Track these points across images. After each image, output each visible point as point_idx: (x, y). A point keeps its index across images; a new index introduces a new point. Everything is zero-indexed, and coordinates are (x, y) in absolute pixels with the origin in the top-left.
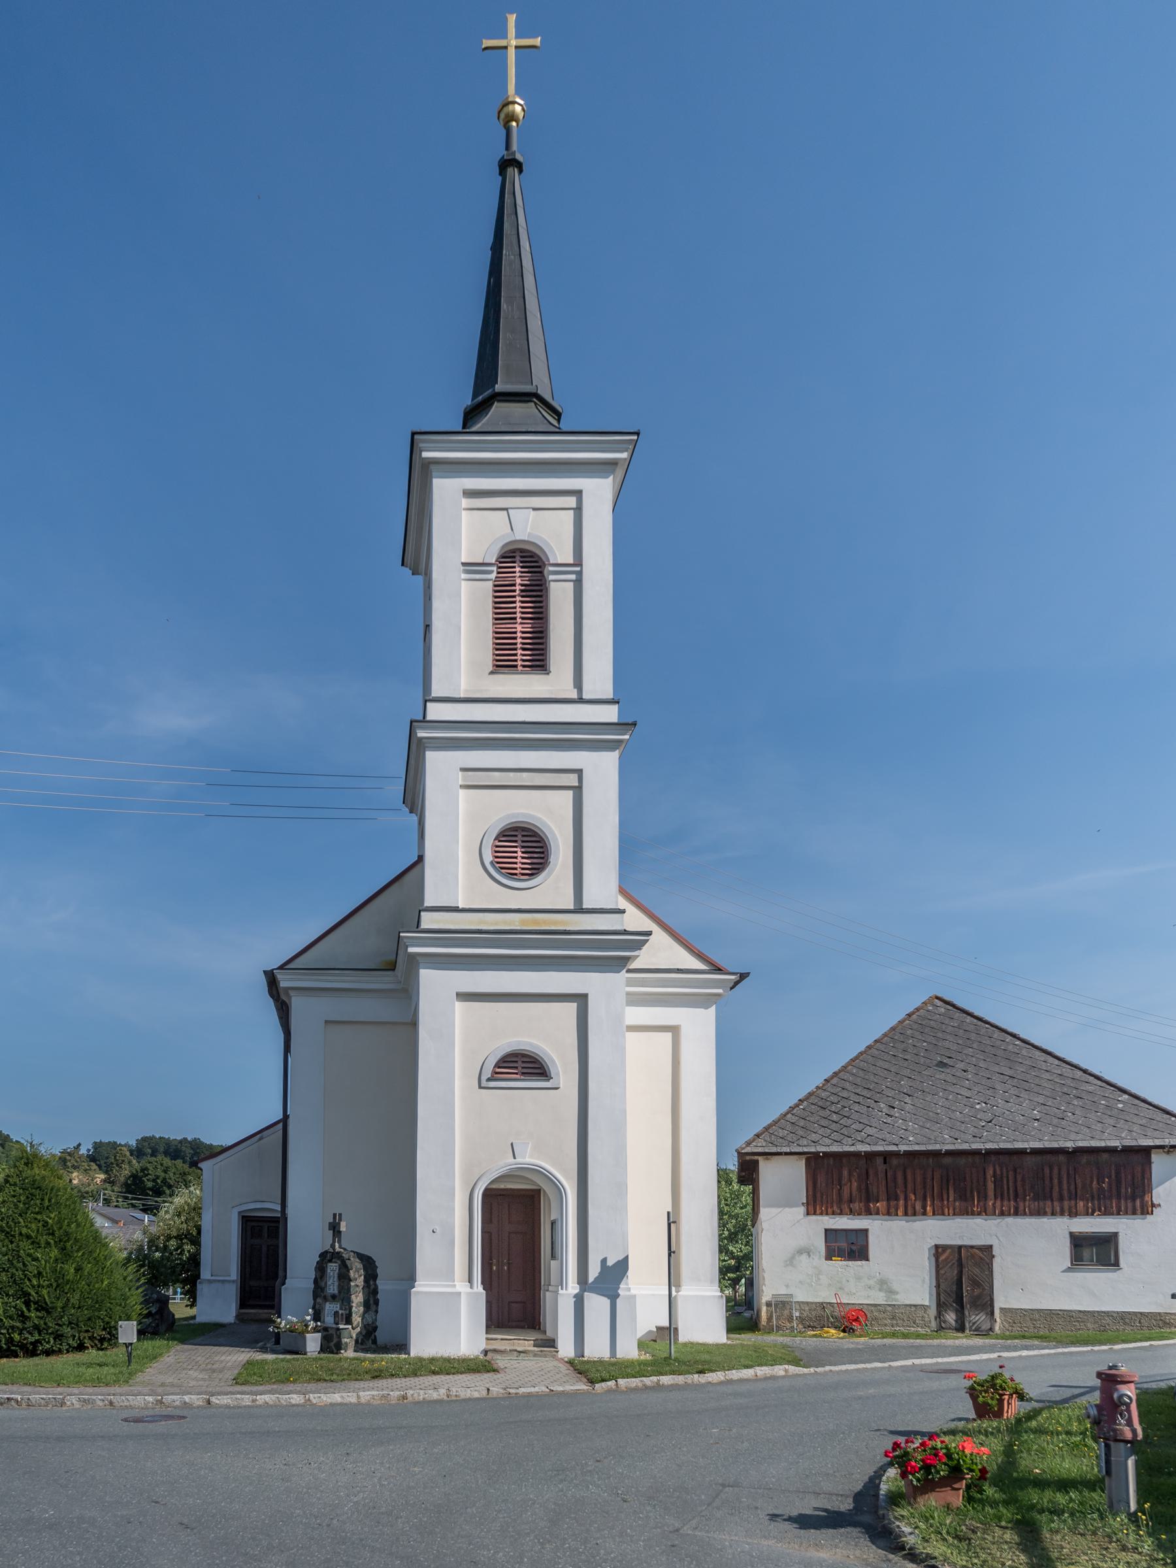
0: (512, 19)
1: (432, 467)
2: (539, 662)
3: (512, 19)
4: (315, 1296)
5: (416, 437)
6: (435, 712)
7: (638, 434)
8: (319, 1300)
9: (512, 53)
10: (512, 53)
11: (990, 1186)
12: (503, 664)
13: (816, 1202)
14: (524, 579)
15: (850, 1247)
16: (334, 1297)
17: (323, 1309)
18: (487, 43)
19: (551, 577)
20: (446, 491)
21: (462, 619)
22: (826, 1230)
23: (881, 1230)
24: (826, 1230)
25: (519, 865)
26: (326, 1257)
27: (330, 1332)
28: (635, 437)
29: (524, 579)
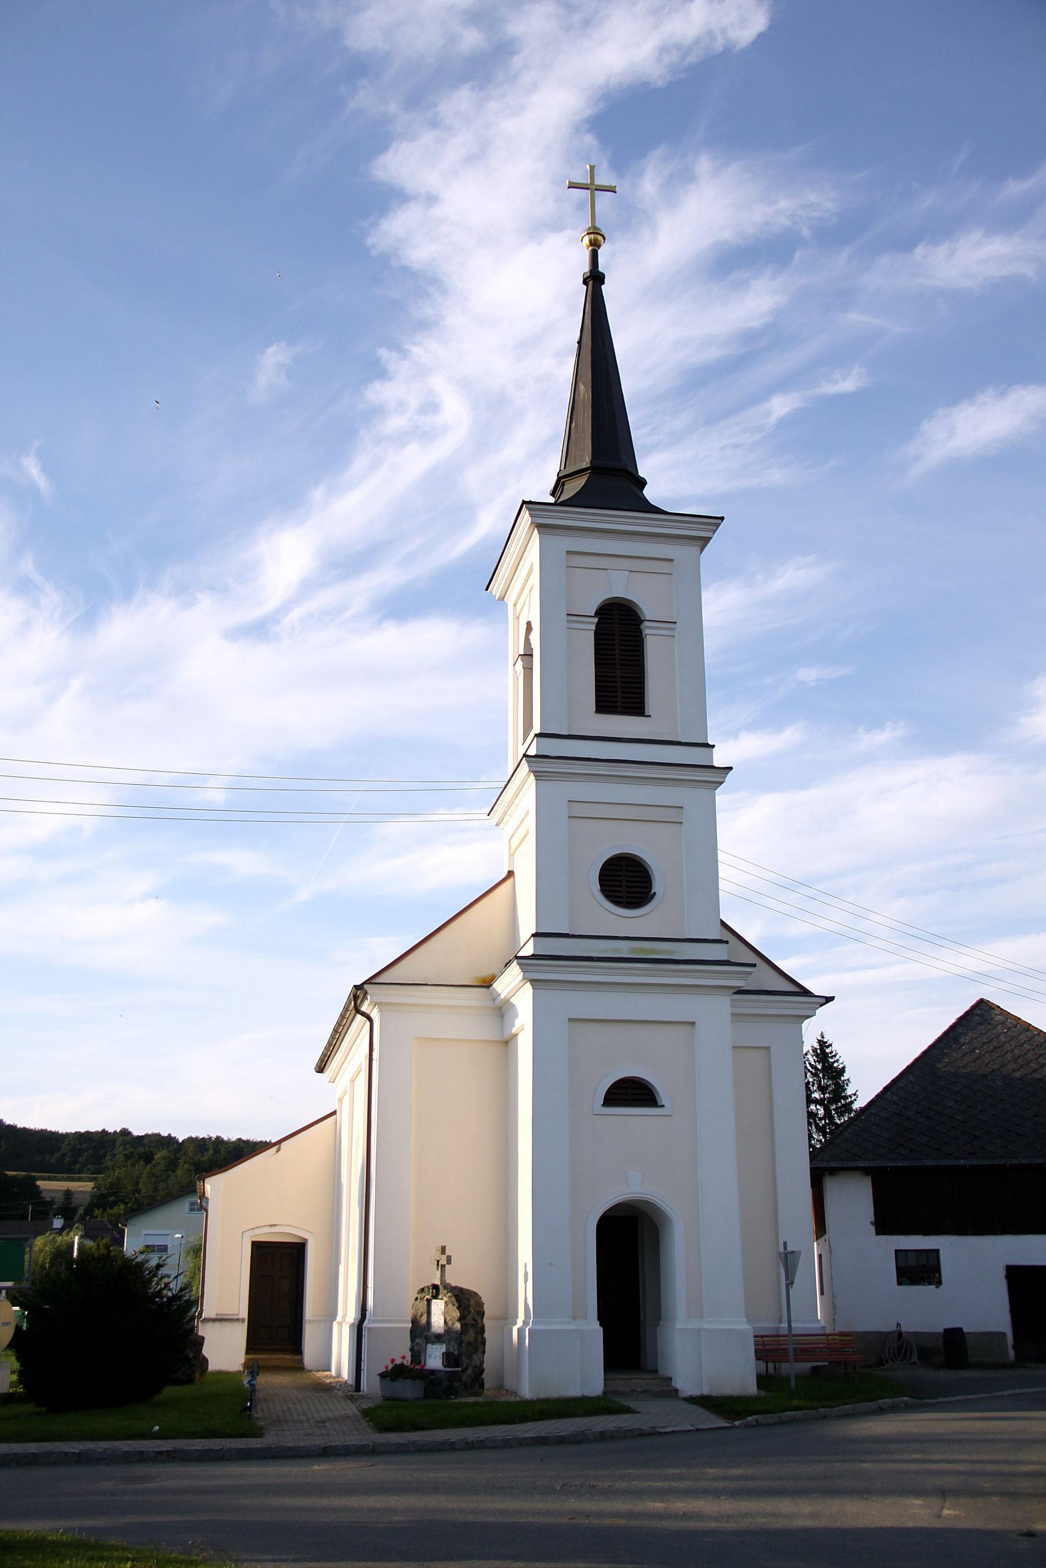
8: (418, 1341)
12: (605, 704)
13: (884, 1224)
15: (918, 1270)
22: (897, 1251)
23: (955, 1251)
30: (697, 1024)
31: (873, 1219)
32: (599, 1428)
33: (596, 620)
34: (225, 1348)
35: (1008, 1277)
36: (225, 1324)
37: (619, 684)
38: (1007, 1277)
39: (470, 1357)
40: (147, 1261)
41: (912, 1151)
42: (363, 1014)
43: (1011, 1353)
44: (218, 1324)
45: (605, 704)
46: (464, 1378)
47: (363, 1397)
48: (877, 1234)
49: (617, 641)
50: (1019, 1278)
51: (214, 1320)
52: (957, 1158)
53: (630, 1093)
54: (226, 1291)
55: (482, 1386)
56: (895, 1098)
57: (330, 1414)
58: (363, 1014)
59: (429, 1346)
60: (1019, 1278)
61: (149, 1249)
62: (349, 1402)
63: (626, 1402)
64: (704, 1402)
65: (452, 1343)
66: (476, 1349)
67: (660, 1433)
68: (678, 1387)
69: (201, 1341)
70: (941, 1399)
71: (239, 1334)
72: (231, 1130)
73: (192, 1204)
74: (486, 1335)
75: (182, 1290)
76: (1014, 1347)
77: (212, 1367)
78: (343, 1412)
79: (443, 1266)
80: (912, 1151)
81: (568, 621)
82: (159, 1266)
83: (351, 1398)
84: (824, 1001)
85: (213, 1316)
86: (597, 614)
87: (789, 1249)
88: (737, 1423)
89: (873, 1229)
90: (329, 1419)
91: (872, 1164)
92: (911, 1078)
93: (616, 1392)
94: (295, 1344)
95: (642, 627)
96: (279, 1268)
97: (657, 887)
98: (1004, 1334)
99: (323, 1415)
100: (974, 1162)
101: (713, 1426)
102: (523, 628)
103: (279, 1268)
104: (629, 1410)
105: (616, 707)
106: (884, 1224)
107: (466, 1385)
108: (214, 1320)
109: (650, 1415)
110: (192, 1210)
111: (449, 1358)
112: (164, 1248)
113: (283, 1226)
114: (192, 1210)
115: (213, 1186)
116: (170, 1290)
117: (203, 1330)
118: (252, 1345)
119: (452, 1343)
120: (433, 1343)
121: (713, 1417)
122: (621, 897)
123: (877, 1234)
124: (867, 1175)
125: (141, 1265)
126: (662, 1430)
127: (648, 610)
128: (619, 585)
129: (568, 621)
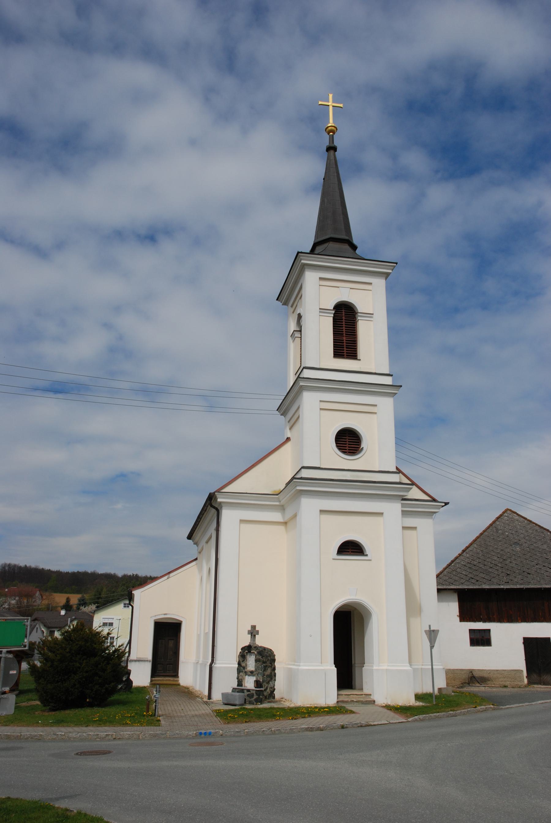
0: (331, 96)
1: (305, 266)
2: (352, 354)
3: (331, 96)
4: (239, 671)
5: (300, 254)
6: (307, 374)
7: (396, 263)
8: (241, 674)
9: (331, 108)
10: (331, 108)
11: (266, 705)
12: (338, 353)
13: (464, 616)
14: (345, 319)
15: (480, 639)
16: (252, 672)
17: (244, 679)
18: (320, 103)
19: (359, 318)
20: (311, 278)
21: (320, 332)
22: (470, 630)
23: (498, 630)
24: (470, 630)
25: (347, 445)
26: (247, 650)
27: (252, 692)
28: (395, 265)
29: (345, 319)
30: (384, 514)
31: (458, 614)
32: (340, 723)
33: (334, 312)
34: (140, 675)
35: (524, 643)
36: (141, 662)
37: (345, 344)
38: (524, 643)
39: (268, 683)
40: (102, 631)
41: (477, 581)
42: (214, 507)
43: (526, 681)
44: (137, 663)
45: (338, 353)
46: (265, 694)
47: (212, 703)
48: (461, 621)
49: (344, 323)
50: (530, 644)
51: (135, 661)
52: (500, 585)
53: (351, 548)
54: (142, 648)
55: (274, 697)
56: (468, 555)
57: (197, 713)
58: (214, 507)
59: (247, 677)
60: (530, 644)
61: (105, 624)
62: (206, 705)
63: (353, 709)
64: (388, 707)
65: (259, 676)
66: (271, 679)
67: (372, 725)
68: (375, 699)
69: (129, 673)
70: (508, 706)
71: (148, 667)
72: (142, 573)
73: (125, 604)
74: (276, 671)
75: (119, 647)
76: (527, 677)
77: (133, 685)
78: (203, 712)
79: (255, 636)
80: (477, 581)
81: (320, 312)
82: (109, 634)
83: (206, 703)
84: (444, 504)
85: (135, 659)
86: (334, 308)
87: (432, 629)
88: (410, 719)
89: (458, 619)
90: (196, 715)
91: (458, 587)
92: (475, 546)
93: (343, 702)
94: (175, 673)
95: (356, 316)
96: (167, 633)
97: (363, 445)
98: (522, 671)
99: (193, 713)
100: (508, 587)
101: (398, 721)
102: (110, 621)
103: (167, 633)
104: (352, 712)
105: (344, 355)
106: (464, 616)
107: (266, 697)
108: (135, 661)
109: (363, 714)
110: (125, 607)
111: (258, 684)
112: (111, 624)
113: (171, 612)
114: (125, 607)
115: (137, 593)
116: (114, 646)
117: (131, 666)
118: (154, 673)
119: (259, 676)
120: (249, 675)
121: (397, 716)
122: (346, 449)
123: (461, 621)
124: (455, 592)
125: (99, 633)
126: (372, 724)
127: (360, 307)
128: (345, 294)
129: (320, 312)
